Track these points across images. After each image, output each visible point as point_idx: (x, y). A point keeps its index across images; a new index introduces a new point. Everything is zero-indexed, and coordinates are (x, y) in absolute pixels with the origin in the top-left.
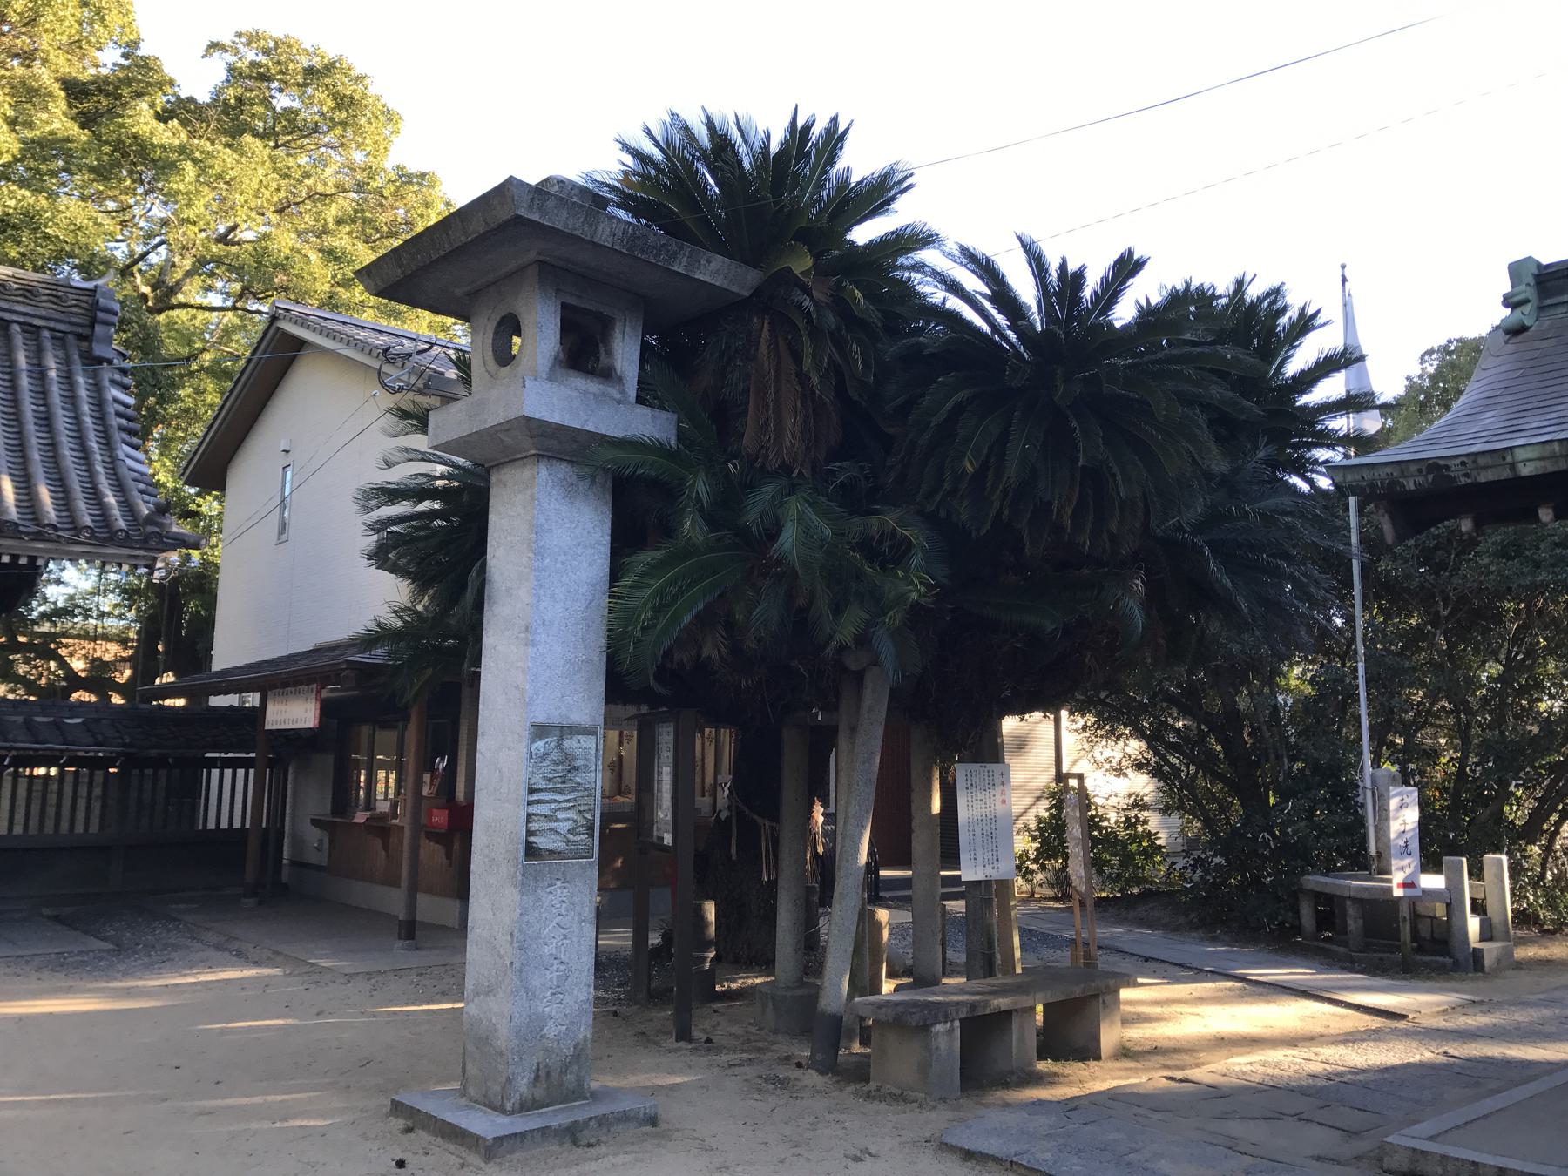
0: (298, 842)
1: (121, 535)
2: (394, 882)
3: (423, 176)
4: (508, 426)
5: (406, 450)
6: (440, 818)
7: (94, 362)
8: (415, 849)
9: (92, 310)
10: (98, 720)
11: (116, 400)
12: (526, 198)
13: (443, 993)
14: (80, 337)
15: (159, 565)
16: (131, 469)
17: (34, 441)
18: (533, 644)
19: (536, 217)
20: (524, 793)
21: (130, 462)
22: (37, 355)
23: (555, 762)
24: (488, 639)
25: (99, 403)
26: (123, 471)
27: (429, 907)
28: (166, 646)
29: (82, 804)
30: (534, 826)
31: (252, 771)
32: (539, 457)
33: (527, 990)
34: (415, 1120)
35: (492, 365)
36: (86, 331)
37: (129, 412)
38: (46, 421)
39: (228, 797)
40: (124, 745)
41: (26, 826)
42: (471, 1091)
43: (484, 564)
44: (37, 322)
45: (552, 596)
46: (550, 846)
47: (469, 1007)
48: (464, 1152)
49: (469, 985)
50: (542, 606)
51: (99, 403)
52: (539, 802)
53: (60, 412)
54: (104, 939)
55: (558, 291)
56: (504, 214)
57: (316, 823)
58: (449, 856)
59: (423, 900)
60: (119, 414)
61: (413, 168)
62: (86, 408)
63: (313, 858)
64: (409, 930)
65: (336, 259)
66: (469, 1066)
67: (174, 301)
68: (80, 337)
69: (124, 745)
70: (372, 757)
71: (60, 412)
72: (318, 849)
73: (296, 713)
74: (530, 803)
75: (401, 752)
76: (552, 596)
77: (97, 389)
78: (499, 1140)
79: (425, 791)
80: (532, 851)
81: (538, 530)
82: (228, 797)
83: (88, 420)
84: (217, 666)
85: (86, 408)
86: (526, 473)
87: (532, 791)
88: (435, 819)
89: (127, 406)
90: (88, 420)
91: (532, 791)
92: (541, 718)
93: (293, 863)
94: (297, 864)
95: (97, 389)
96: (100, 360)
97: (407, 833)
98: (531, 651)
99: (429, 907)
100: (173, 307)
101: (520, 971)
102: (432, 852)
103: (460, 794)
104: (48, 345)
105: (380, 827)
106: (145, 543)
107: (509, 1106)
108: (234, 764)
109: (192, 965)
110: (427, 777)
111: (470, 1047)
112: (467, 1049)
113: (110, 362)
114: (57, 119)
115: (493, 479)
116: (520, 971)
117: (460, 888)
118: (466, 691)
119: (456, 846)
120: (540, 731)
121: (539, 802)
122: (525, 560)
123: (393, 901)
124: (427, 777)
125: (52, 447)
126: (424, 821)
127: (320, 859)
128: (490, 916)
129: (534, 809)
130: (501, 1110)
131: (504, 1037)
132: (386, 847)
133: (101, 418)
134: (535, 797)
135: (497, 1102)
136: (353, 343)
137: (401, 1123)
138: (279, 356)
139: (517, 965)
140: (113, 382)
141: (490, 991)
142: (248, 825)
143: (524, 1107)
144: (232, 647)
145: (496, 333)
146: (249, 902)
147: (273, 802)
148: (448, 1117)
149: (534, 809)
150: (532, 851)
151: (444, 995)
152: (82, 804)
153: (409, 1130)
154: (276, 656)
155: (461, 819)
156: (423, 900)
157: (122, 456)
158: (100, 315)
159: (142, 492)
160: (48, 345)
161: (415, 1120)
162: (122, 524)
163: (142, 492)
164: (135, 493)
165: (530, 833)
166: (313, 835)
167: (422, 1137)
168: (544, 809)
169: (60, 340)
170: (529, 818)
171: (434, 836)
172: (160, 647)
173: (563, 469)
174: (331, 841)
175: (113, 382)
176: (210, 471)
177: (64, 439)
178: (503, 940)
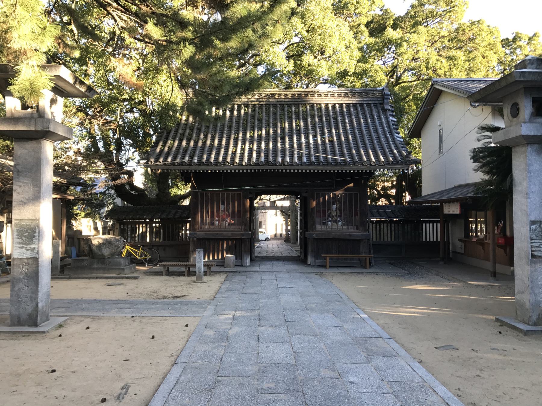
0: (454, 246)
1: (400, 162)
2: (487, 259)
3: (479, 22)
4: (517, 137)
5: (484, 136)
6: (502, 241)
7: (385, 111)
8: (494, 250)
9: (383, 96)
10: (395, 210)
11: (392, 120)
12: (519, 75)
13: (507, 294)
14: (381, 104)
15: (410, 169)
16: (398, 141)
17: (374, 137)
18: (529, 198)
19: (522, 79)
20: (529, 240)
21: (398, 139)
22: (371, 111)
23: (539, 231)
24: (514, 197)
25: (388, 123)
26: (397, 142)
27: (500, 268)
28: (406, 183)
29: (389, 232)
30: (533, 249)
31: (439, 224)
32: (527, 144)
33: (534, 293)
34: (503, 324)
35: (511, 118)
36: (382, 102)
37: (396, 123)
38: (376, 131)
39: (431, 232)
40: (403, 217)
41: (376, 239)
42: (519, 318)
43: (512, 175)
44: (370, 102)
45: (534, 184)
46: (539, 255)
47: (518, 297)
48: (518, 333)
49: (516, 291)
50: (531, 187)
51: (388, 123)
52: (534, 242)
53: (379, 127)
54: (405, 270)
55: (531, 95)
56: (511, 80)
57: (459, 240)
58: (505, 252)
59: (498, 266)
60: (393, 125)
61: (475, 19)
62: (385, 125)
63: (459, 251)
64: (494, 275)
65: (451, 59)
66: (518, 312)
67: (400, 81)
68: (381, 104)
69: (403, 217)
70: (476, 220)
71: (379, 127)
72: (461, 248)
73: (454, 209)
74: (531, 243)
75: (486, 218)
76: (534, 184)
77: (387, 118)
78: (528, 331)
79: (496, 232)
80: (533, 256)
81: (528, 165)
82: (431, 232)
83: (386, 128)
84: (424, 194)
85: (385, 125)
86: (524, 149)
87: (532, 239)
88: (500, 241)
89: (394, 121)
90: (386, 128)
91: (532, 239)
92: (533, 219)
93: (453, 252)
94: (455, 252)
95: (387, 118)
96: (386, 110)
97: (491, 246)
98: (529, 200)
99: (500, 268)
100: (400, 83)
101: (532, 288)
102: (500, 252)
103: (508, 233)
104: (373, 108)
105: (481, 242)
106: (406, 163)
107: (530, 323)
108: (433, 222)
109: (417, 284)
110: (496, 228)
111: (517, 307)
112: (518, 306)
113: (389, 110)
114: (366, 39)
115: (513, 150)
116: (532, 288)
117: (511, 262)
118: (508, 203)
119: (508, 250)
120: (533, 223)
121: (534, 242)
122: (525, 174)
123: (488, 265)
124: (496, 228)
125: (379, 138)
126: (496, 242)
127: (462, 251)
128: (521, 272)
129: (533, 244)
130: (528, 324)
131: (528, 305)
132: (483, 249)
133: (389, 127)
134: (533, 241)
135: (527, 322)
136: (462, 92)
137: (499, 324)
138: (435, 95)
139: (530, 286)
140: (390, 115)
141: (523, 293)
142: (439, 240)
143: (535, 324)
144: (428, 188)
145: (511, 108)
146: (442, 263)
147: (445, 233)
148: (513, 324)
149: (533, 244)
150: (533, 256)
151: (508, 295)
152: (389, 232)
153: (501, 326)
154: (442, 190)
155: (509, 242)
156: (498, 266)
157: (396, 137)
158: (385, 97)
159: (402, 147)
160: (373, 108)
161: (503, 324)
162: (399, 158)
163: (402, 147)
164: (401, 148)
165: (532, 251)
166: (459, 244)
167: (505, 328)
168: (536, 245)
169: (376, 106)
170: (532, 247)
171: (500, 246)
172: (404, 183)
173: (536, 146)
174: (465, 246)
175: (390, 115)
176: (416, 132)
177: (381, 135)
178: (526, 280)
